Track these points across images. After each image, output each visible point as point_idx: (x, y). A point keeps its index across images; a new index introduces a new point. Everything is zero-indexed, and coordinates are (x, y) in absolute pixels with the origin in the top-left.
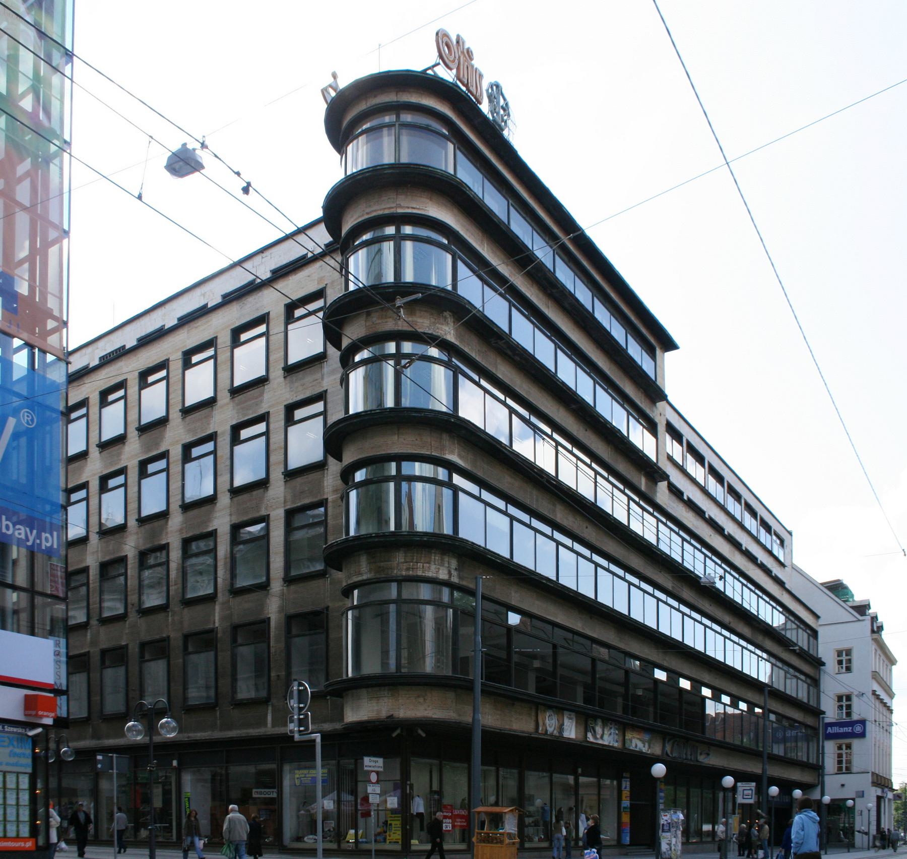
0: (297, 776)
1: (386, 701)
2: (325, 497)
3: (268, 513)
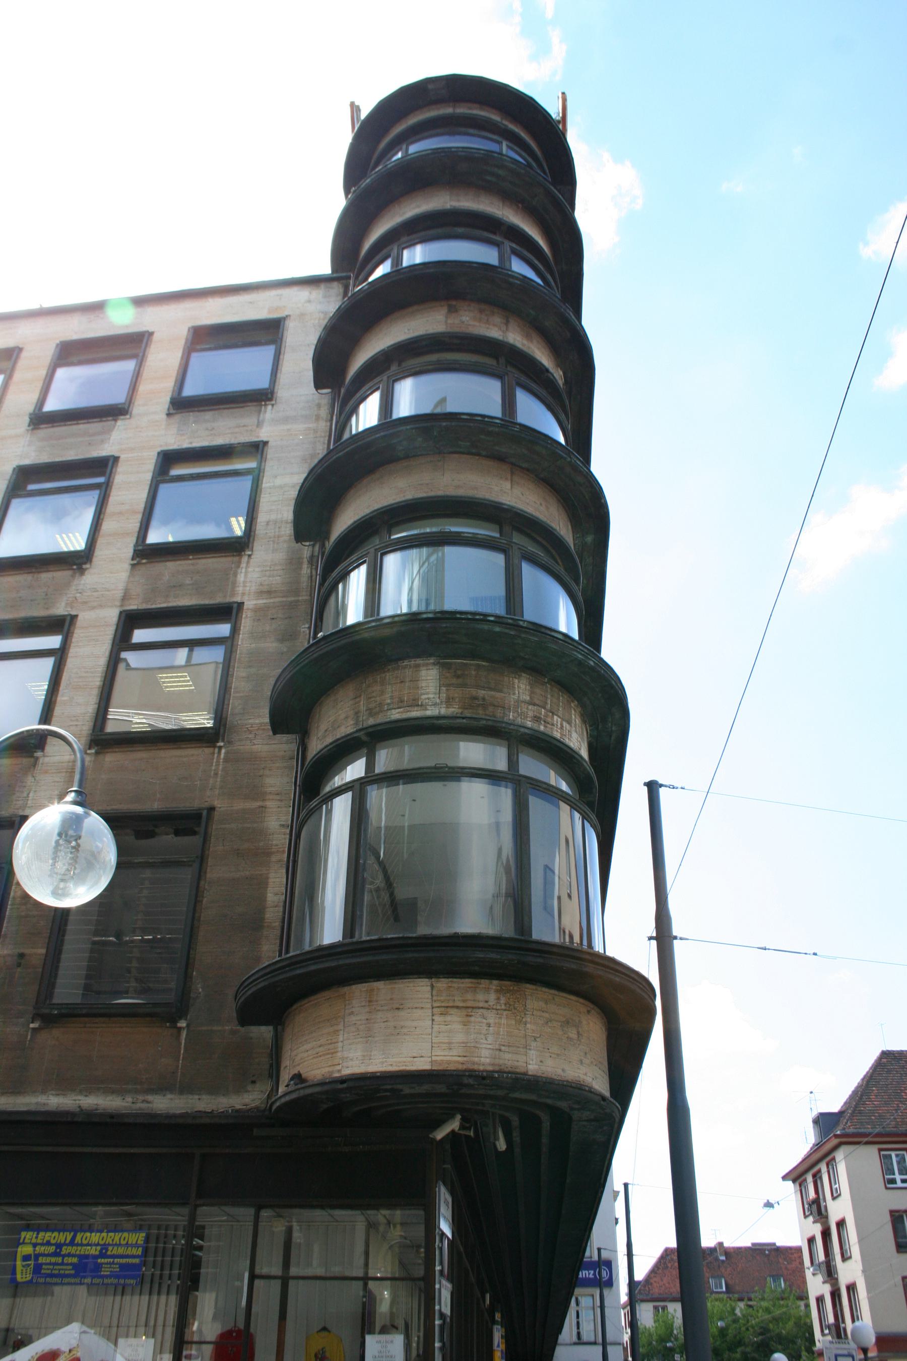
0: (27, 1250)
1: (491, 1021)
2: (238, 599)
3: (74, 613)
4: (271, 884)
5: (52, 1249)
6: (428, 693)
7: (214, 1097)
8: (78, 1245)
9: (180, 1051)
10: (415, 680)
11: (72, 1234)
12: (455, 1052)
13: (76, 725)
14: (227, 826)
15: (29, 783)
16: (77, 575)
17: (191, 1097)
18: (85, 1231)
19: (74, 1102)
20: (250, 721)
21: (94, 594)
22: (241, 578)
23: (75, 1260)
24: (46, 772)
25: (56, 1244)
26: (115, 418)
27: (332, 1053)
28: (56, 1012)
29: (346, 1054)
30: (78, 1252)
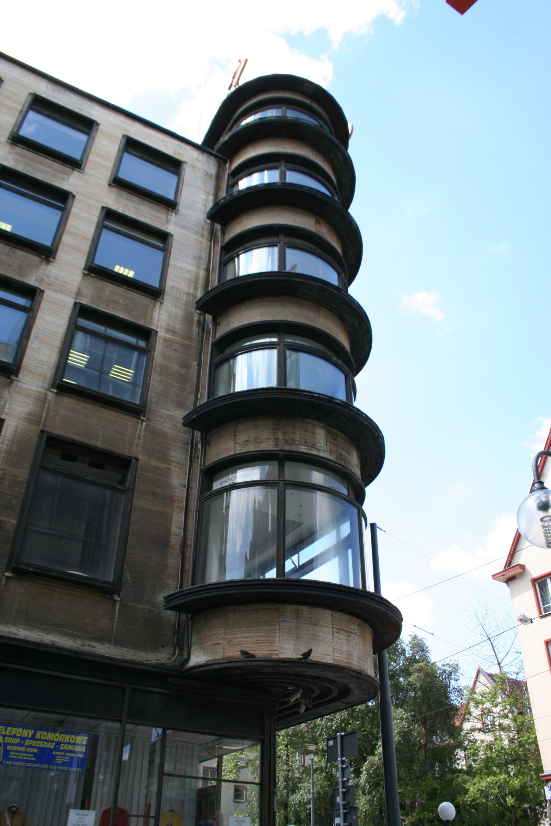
4: (174, 521)
5: (18, 741)
6: (320, 443)
7: (137, 651)
8: (37, 740)
9: (115, 617)
10: (313, 433)
11: (33, 731)
12: (343, 656)
13: (43, 368)
14: (146, 474)
15: (5, 396)
16: (44, 263)
17: (122, 648)
18: (43, 731)
19: (38, 636)
20: (162, 410)
21: (56, 281)
22: (156, 315)
23: (35, 750)
24: (19, 393)
25: (20, 737)
26: (73, 168)
27: (271, 643)
28: (32, 570)
29: (282, 645)
30: (38, 745)
